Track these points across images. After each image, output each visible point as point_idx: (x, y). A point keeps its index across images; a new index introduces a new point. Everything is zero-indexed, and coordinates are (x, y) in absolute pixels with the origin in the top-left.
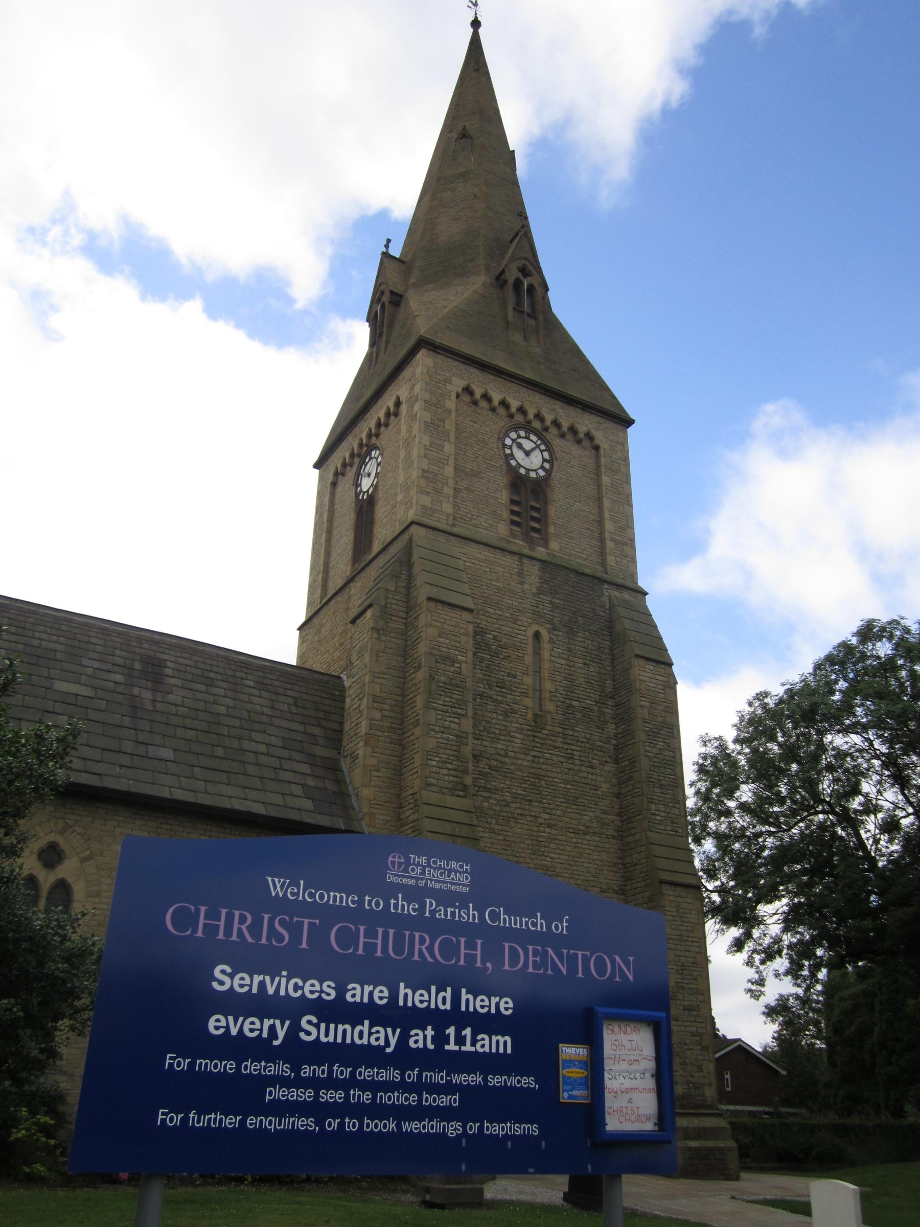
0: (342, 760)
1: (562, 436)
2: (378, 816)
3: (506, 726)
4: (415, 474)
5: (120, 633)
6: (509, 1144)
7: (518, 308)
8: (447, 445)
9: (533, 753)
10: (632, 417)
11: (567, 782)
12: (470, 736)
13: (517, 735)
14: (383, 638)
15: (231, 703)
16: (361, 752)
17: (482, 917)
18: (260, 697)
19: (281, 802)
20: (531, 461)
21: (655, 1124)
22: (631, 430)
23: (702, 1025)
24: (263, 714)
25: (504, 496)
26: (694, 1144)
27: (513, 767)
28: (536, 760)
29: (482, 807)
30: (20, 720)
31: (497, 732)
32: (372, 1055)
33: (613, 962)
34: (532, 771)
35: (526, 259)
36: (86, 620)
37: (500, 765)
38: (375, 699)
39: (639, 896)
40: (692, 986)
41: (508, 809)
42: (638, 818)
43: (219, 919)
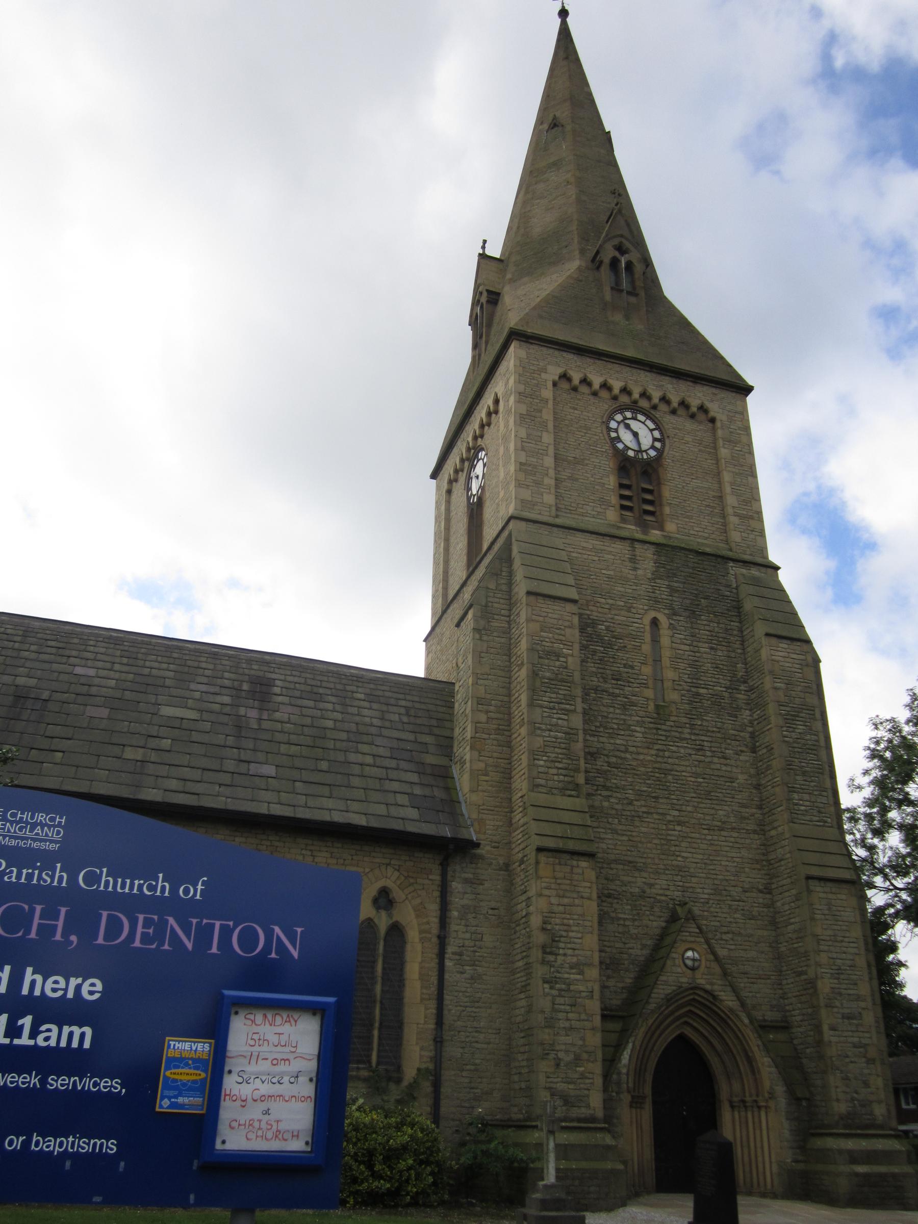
0: (453, 767)
1: (674, 412)
2: (488, 822)
3: (624, 720)
4: (512, 468)
5: (230, 657)
6: (68, 1164)
7: (616, 288)
8: (544, 434)
9: (656, 747)
10: (751, 383)
11: (697, 775)
12: (581, 732)
13: (638, 729)
14: (485, 638)
15: (339, 716)
16: (467, 757)
17: (73, 879)
18: (371, 709)
19: (385, 813)
20: (638, 435)
21: (307, 1143)
22: (750, 399)
23: (867, 1035)
24: (372, 725)
25: (612, 481)
26: (861, 1169)
27: (634, 763)
28: (661, 754)
30: (124, 746)
31: (616, 727)
33: (269, 934)
34: (657, 765)
35: (622, 236)
36: (198, 647)
38: (480, 701)
39: (787, 894)
40: (851, 992)
41: (631, 808)
42: (779, 809)
43: (57, 919)
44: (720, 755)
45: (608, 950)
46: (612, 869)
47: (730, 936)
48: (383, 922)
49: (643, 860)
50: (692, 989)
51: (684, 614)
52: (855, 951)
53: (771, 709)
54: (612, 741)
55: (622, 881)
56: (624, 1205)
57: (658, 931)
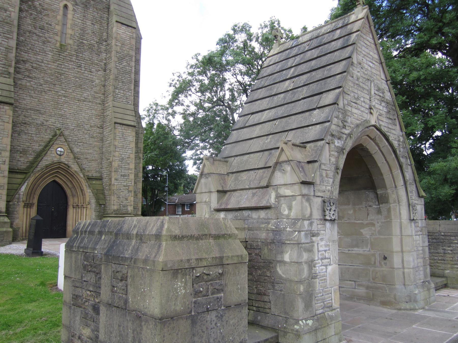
9: (58, 62)
13: (50, 53)
27: (46, 68)
28: (60, 66)
29: (26, 85)
31: (38, 50)
34: (57, 71)
37: (38, 66)
39: (108, 129)
41: (41, 87)
44: (89, 70)
45: (22, 146)
46: (28, 112)
47: (82, 144)
49: (45, 110)
50: (58, 163)
51: (81, 5)
52: (131, 152)
53: (113, 53)
54: (35, 57)
55: (33, 118)
56: (10, 244)
57: (48, 140)
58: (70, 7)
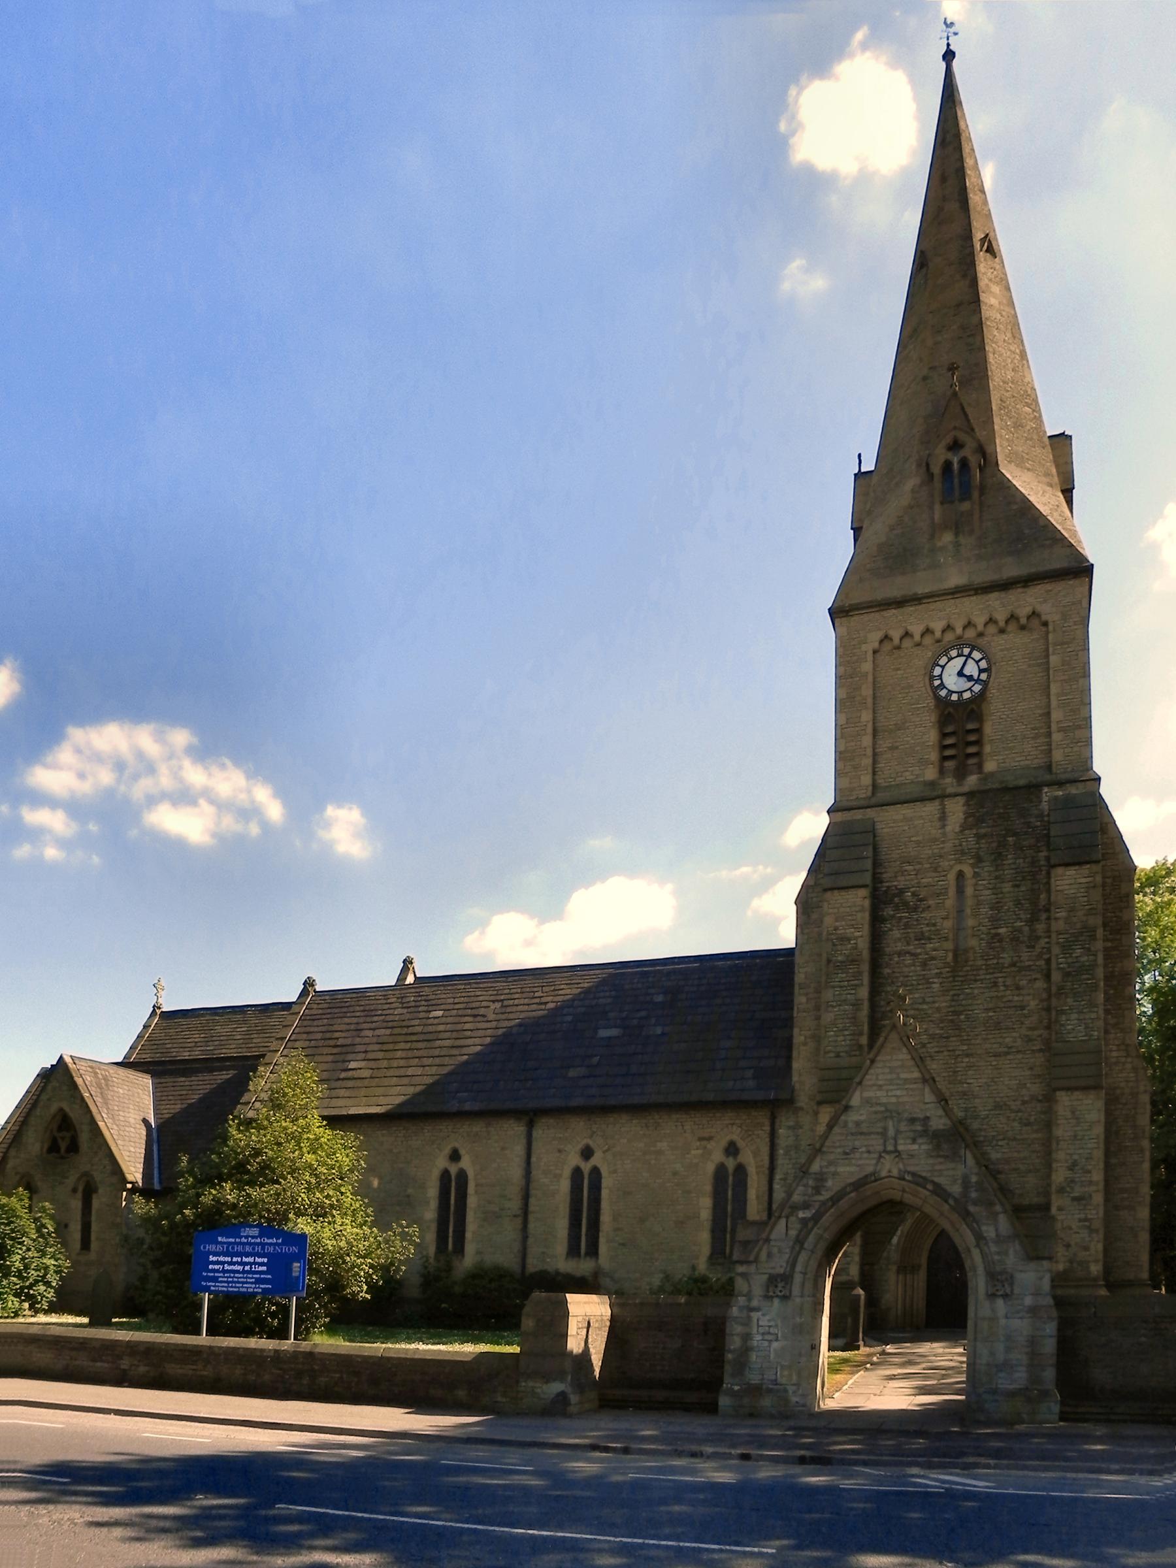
9: (952, 993)
11: (988, 1010)
14: (806, 931)
25: (932, 736)
32: (238, 1272)
35: (955, 428)
48: (731, 1164)
58: (968, 871)
